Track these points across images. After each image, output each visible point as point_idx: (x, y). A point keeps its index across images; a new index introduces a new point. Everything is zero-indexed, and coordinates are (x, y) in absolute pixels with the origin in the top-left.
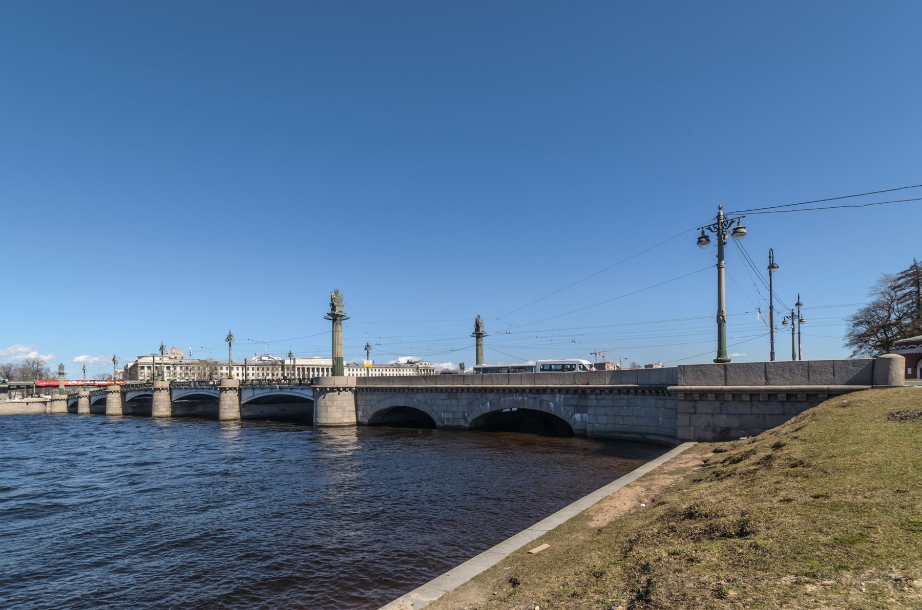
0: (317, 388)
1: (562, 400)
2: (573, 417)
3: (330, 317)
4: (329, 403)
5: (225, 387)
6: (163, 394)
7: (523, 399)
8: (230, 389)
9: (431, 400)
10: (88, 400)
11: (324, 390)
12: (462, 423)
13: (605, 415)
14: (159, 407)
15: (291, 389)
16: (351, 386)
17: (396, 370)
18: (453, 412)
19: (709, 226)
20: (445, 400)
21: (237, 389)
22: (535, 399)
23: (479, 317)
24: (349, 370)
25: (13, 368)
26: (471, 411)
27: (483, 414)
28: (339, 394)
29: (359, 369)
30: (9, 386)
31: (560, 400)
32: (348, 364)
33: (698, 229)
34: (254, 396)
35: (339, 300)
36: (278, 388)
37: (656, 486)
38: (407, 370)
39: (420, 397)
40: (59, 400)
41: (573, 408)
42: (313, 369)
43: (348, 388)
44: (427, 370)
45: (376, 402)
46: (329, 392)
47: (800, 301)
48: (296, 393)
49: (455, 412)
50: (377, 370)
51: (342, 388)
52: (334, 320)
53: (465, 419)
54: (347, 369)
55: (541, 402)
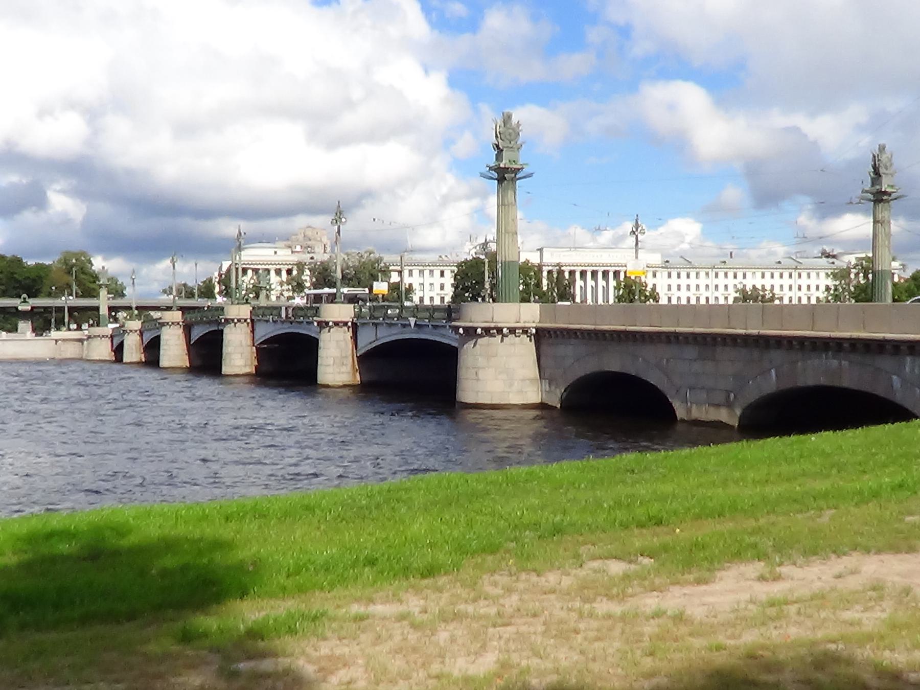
0: (460, 327)
4: (481, 361)
5: (327, 320)
6: (239, 331)
7: (840, 364)
8: (336, 324)
9: (667, 360)
10: (138, 338)
11: (471, 331)
14: (233, 356)
15: (435, 327)
16: (527, 325)
17: (790, 276)
21: (350, 324)
23: (882, 149)
24: (670, 276)
28: (502, 341)
29: (693, 275)
30: (33, 308)
32: (667, 262)
34: (377, 340)
35: (510, 134)
36: (413, 325)
38: (818, 274)
39: (649, 352)
40: (99, 336)
42: (583, 274)
43: (519, 328)
46: (481, 336)
50: (731, 275)
51: (508, 328)
52: (501, 180)
54: (666, 274)
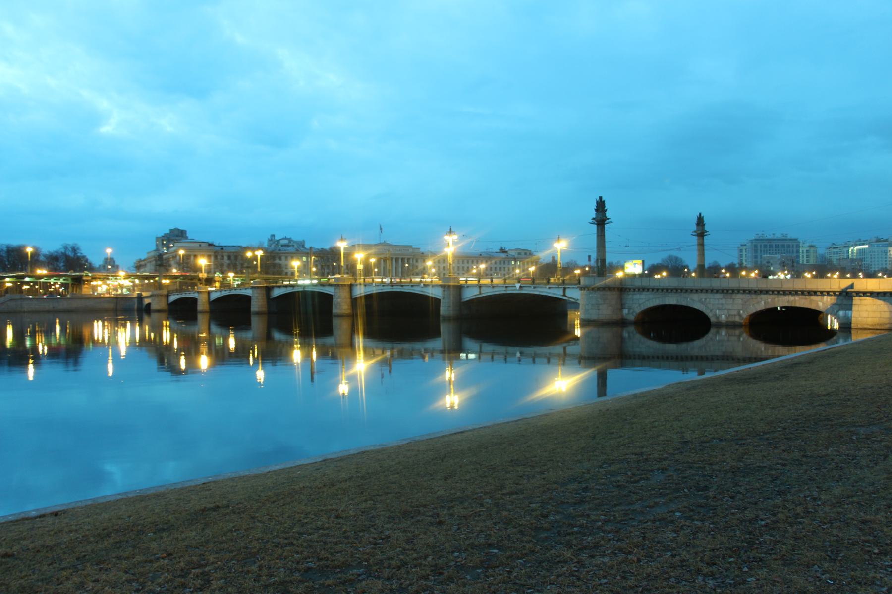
3: (694, 233)
12: (737, 319)
37: (252, 574)
39: (695, 296)
48: (542, 292)
49: (730, 310)
53: (739, 315)
55: (811, 301)
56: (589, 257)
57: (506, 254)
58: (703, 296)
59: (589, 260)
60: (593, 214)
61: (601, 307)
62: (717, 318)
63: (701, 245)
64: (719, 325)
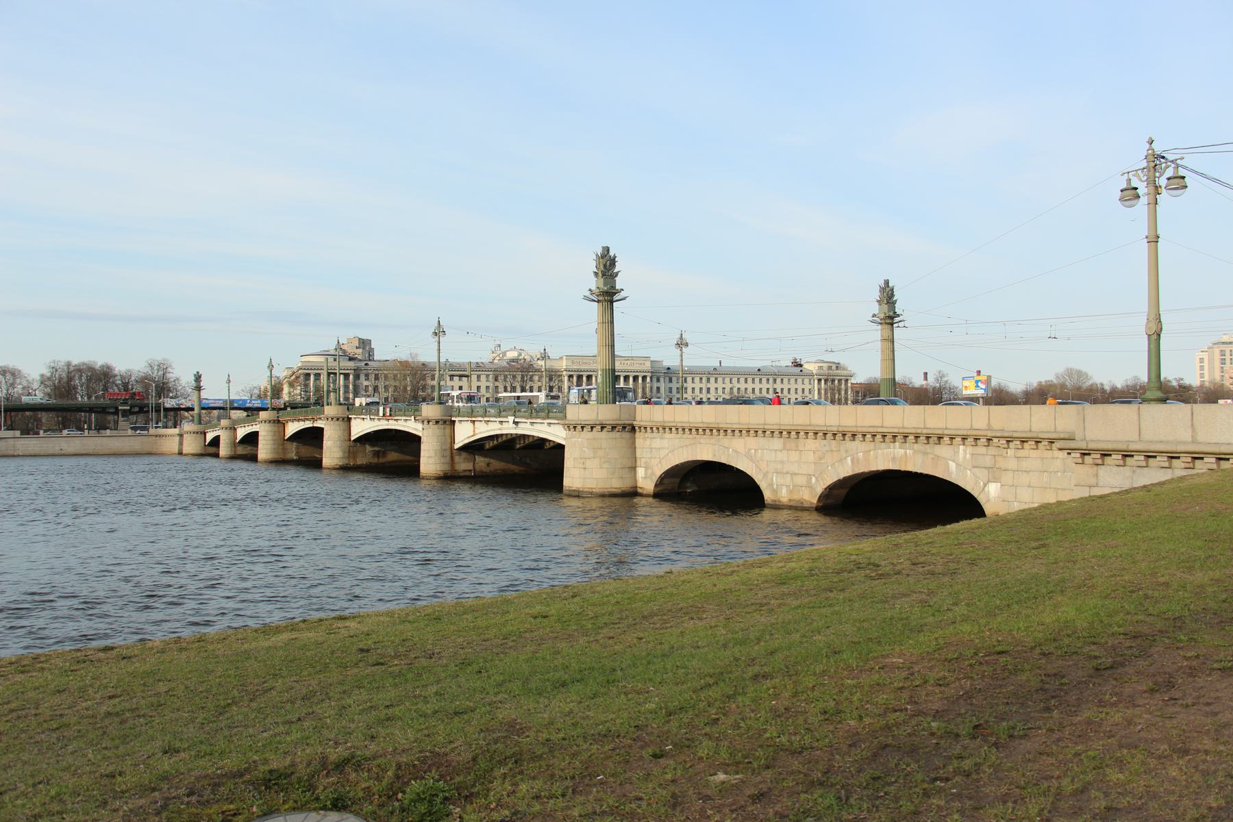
1: (968, 456)
2: (986, 489)
13: (1029, 486)
18: (791, 474)
19: (1137, 171)
20: (778, 452)
22: (925, 453)
25: (133, 378)
26: (821, 473)
27: (839, 480)
31: (965, 458)
33: (1122, 175)
41: (986, 472)
44: (833, 381)
45: (667, 451)
47: (325, 470)
49: (795, 474)
53: (810, 487)
56: (926, 374)
57: (800, 369)
58: (751, 442)
59: (926, 378)
60: (594, 283)
61: (588, 464)
62: (775, 492)
63: (609, 322)
64: (777, 507)
